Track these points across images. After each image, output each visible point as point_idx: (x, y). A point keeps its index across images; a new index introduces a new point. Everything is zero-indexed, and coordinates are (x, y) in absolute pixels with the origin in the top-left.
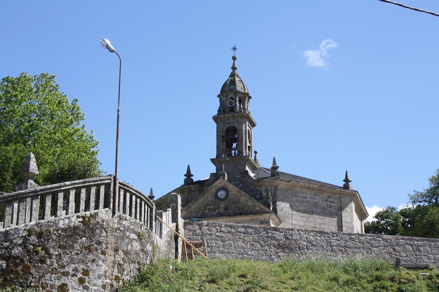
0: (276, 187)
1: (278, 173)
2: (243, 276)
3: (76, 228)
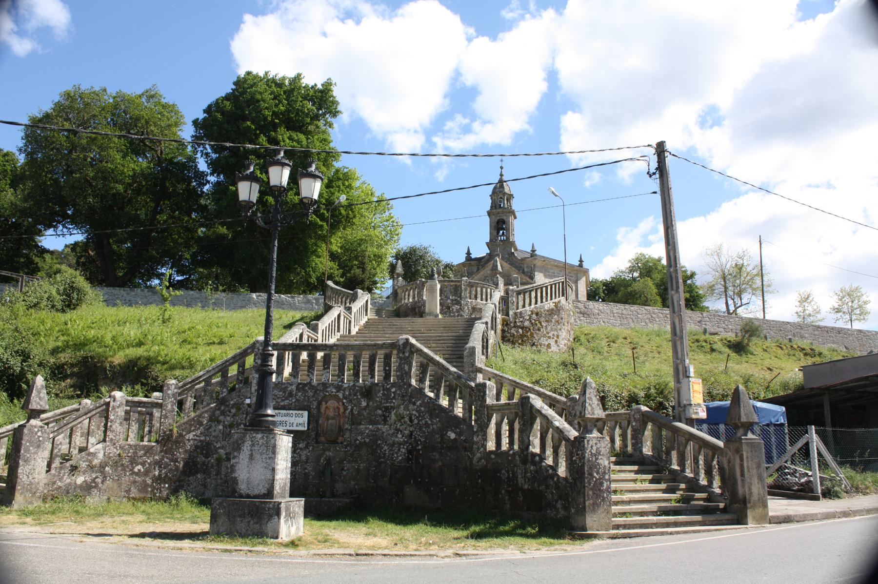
0: (534, 265)
1: (536, 255)
2: (625, 338)
3: (552, 310)
